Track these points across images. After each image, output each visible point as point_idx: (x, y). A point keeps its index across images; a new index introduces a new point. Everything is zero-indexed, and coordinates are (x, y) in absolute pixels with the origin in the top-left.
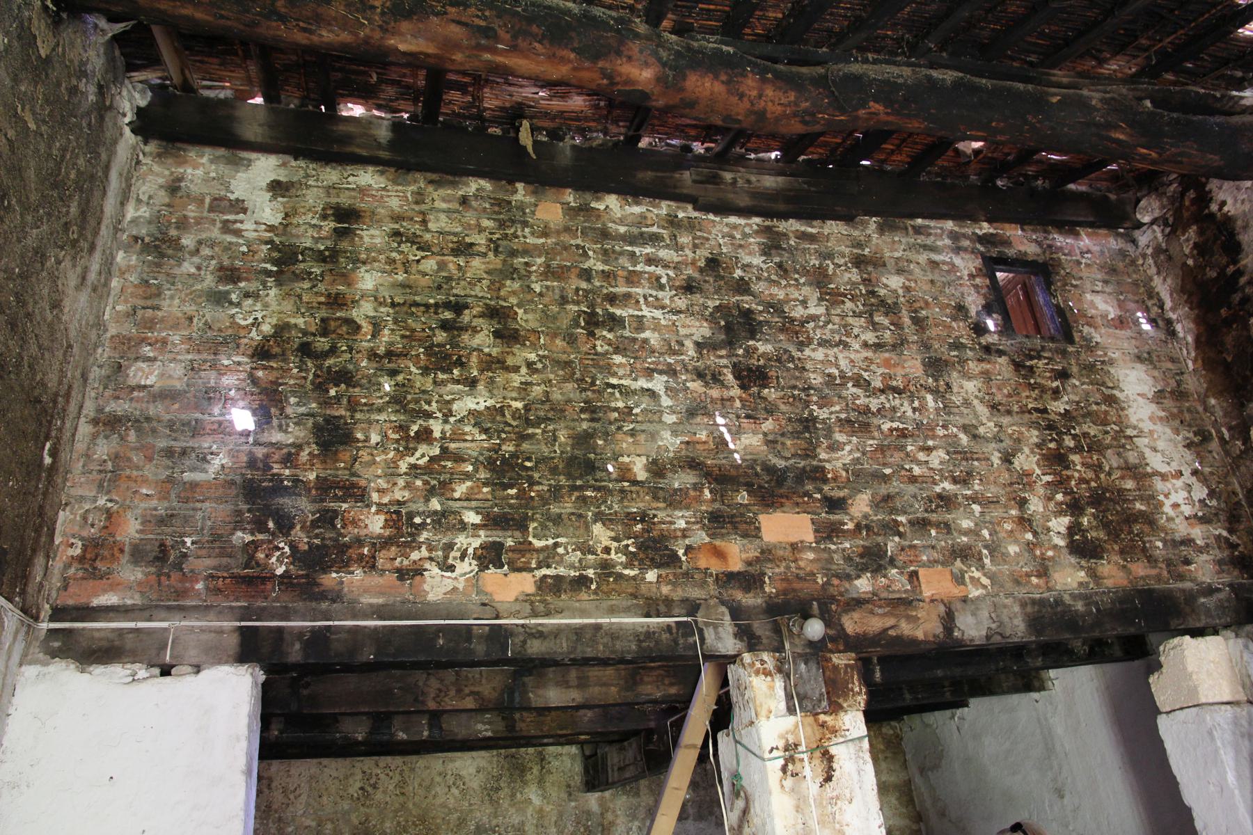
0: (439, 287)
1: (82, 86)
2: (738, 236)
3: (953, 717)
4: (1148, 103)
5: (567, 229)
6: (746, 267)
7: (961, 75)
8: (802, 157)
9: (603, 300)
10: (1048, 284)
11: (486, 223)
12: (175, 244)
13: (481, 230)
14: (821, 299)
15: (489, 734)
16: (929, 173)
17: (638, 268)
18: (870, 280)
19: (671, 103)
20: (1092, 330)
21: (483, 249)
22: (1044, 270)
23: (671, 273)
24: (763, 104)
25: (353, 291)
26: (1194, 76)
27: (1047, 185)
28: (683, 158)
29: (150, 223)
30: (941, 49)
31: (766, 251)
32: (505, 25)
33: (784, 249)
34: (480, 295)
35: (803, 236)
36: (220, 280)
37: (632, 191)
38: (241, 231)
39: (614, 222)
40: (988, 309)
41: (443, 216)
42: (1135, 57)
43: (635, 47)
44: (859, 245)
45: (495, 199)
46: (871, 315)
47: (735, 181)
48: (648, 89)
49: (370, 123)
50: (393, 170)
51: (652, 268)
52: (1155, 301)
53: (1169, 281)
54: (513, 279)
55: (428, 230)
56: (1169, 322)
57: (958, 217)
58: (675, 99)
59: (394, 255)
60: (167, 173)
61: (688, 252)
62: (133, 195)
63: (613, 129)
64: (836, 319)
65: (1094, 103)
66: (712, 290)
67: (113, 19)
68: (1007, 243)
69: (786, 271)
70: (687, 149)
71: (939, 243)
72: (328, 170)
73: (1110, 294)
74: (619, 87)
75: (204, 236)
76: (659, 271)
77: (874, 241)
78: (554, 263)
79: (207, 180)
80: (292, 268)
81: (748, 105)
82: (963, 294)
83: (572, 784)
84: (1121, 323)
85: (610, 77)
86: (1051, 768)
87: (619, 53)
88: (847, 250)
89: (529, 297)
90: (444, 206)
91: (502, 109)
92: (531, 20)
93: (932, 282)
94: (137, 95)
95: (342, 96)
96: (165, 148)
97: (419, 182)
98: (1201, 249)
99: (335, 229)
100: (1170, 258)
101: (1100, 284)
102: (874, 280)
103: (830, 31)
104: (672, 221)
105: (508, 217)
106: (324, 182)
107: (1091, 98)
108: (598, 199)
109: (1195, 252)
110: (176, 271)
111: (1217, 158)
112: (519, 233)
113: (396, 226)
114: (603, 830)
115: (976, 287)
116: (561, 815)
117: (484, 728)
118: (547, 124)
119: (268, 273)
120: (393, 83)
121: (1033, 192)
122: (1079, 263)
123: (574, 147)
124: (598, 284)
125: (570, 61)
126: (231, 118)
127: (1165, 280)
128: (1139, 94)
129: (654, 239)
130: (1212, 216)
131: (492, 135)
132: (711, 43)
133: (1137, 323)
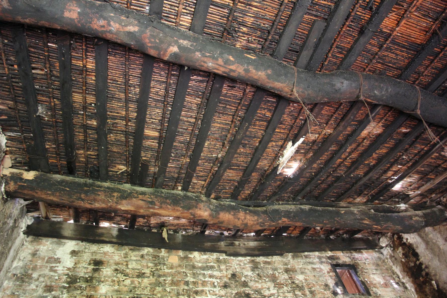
0: (131, 291)
1: (8, 221)
2: (242, 265)
4: (372, 211)
5: (180, 266)
6: (246, 276)
7: (311, 206)
8: (262, 234)
9: (193, 293)
10: (356, 273)
11: (150, 265)
12: (30, 277)
13: (148, 267)
14: (275, 287)
16: (307, 236)
17: (206, 279)
18: (292, 278)
19: (215, 222)
20: (376, 289)
21: (148, 275)
22: (353, 267)
23: (219, 281)
24: (246, 221)
25: (97, 294)
26: (385, 201)
27: (347, 236)
28: (220, 238)
29: (22, 268)
30: (303, 198)
31: (253, 270)
32: (158, 200)
33: (259, 268)
34: (146, 294)
35: (266, 263)
36: (45, 291)
37: (203, 250)
38: (57, 270)
39: (197, 262)
40: (337, 284)
41: (134, 263)
42: (364, 197)
43: (202, 205)
44: (286, 264)
45: (153, 255)
46: (294, 292)
47: (239, 245)
48: (207, 218)
49: (111, 229)
50: (117, 245)
51: (211, 279)
52: (396, 275)
54: (159, 286)
55: (128, 268)
56: (403, 283)
57: (320, 250)
58: (216, 221)
59: (115, 278)
60: (33, 248)
61: (224, 272)
62: (18, 257)
63: (196, 228)
64: (281, 294)
65: (355, 212)
66: (234, 286)
67: (25, 200)
68: (338, 258)
69: (261, 277)
70: (222, 234)
71: (315, 261)
72: (93, 246)
73: (379, 274)
74: (197, 218)
75: (42, 273)
76: (214, 280)
77: (291, 262)
78: (175, 279)
79: (47, 251)
80: (74, 285)
81: (241, 222)
82: (326, 280)
84: (386, 285)
85: (194, 215)
87: (196, 207)
88: (282, 267)
89: (165, 293)
90: (135, 258)
91: (157, 223)
92: (166, 198)
93: (314, 276)
94: (28, 221)
95: (101, 220)
96: (35, 239)
97: (126, 249)
99: (93, 269)
100: (396, 259)
101: (375, 271)
102: (293, 277)
103: (266, 196)
104: (218, 261)
105: (158, 261)
106: (92, 250)
107: (354, 211)
108: (191, 254)
110: (28, 288)
111: (399, 227)
112: (162, 268)
113: (116, 267)
115: (330, 276)
118: (173, 228)
119: (64, 287)
120: (119, 216)
121: (343, 239)
122: (365, 263)
123: (182, 235)
124: (191, 287)
125: (180, 211)
126: (61, 228)
127: (397, 267)
128: (369, 208)
129: (212, 267)
130: (405, 244)
131: (153, 232)
132: (227, 202)
133: (392, 285)
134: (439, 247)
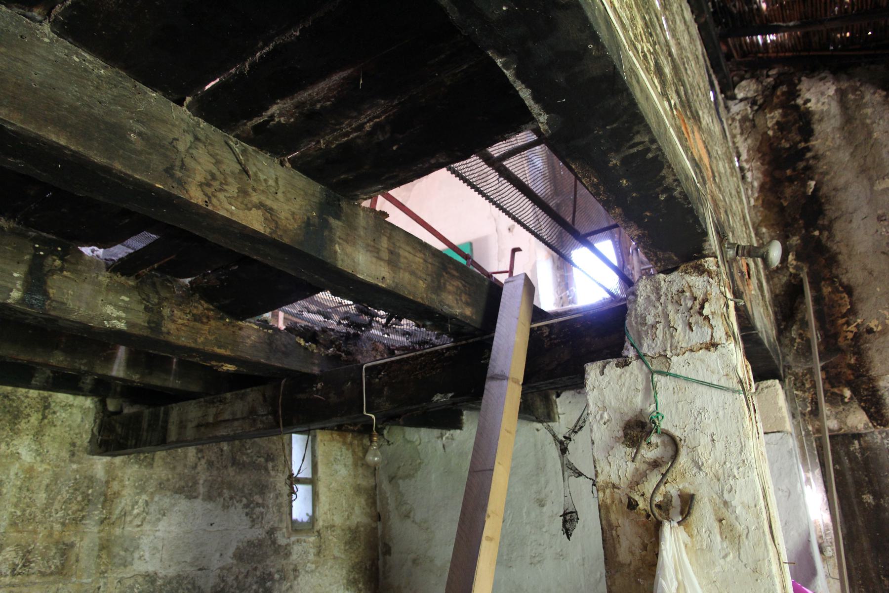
3: (442, 436)
15: (122, 325)
53: (749, 141)
83: (79, 443)
86: (538, 483)
98: (781, 126)
100: (754, 126)
109: (776, 127)
114: (105, 501)
116: (56, 478)
117: (116, 313)
127: (746, 139)
130: (797, 107)
134: (870, 134)
